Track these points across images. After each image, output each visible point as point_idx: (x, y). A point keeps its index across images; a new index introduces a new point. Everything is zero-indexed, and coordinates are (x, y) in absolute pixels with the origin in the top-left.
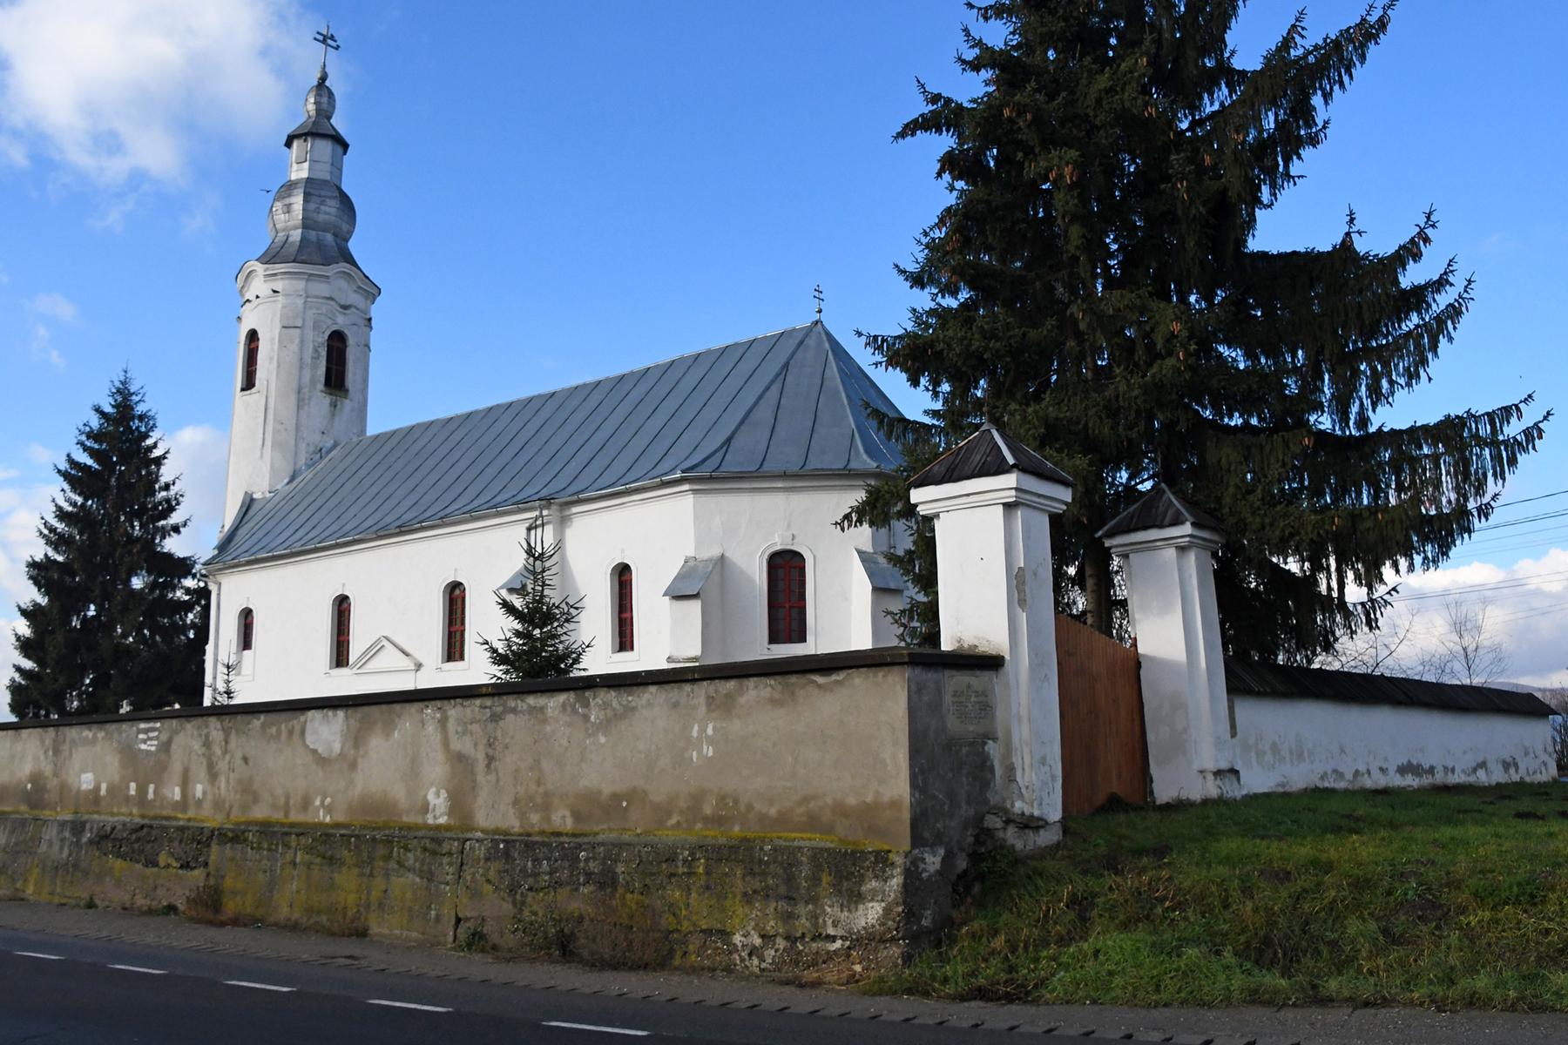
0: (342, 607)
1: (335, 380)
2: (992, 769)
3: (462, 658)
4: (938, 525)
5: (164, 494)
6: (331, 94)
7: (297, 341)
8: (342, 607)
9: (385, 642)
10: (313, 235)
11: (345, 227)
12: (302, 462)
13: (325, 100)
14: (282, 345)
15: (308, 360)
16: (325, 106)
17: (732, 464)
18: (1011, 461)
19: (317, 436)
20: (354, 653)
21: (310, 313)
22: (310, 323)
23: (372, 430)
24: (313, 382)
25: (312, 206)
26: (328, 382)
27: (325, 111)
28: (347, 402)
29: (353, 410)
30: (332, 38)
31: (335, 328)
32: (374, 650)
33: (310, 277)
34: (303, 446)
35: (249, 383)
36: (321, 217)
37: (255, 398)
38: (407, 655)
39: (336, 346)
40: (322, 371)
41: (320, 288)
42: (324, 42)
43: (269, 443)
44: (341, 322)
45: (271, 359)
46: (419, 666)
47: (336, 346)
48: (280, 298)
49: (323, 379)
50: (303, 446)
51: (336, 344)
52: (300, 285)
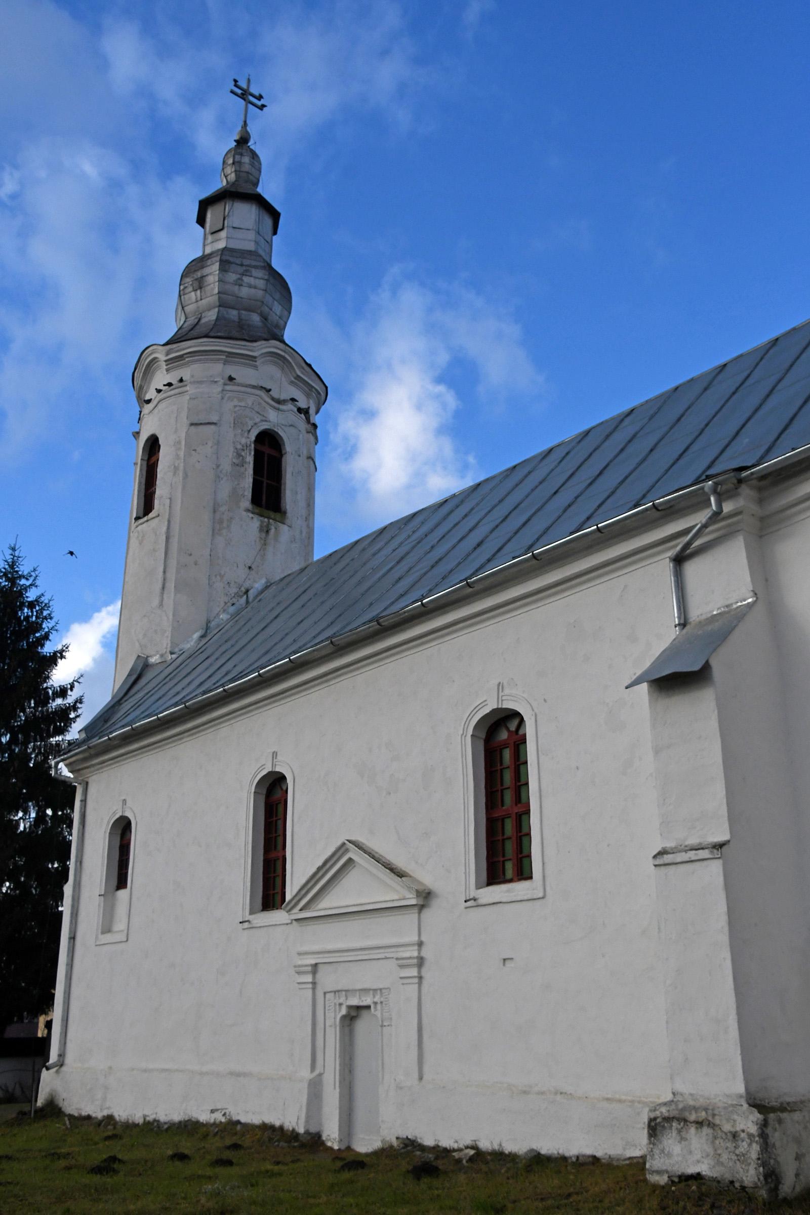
0: (273, 793)
1: (268, 496)
3: (523, 873)
5: (59, 701)
6: (254, 155)
8: (273, 793)
9: (353, 853)
10: (233, 314)
11: (278, 309)
13: (246, 160)
14: (191, 449)
15: (226, 466)
16: (247, 167)
18: (66, 1119)
19: (242, 573)
20: (297, 875)
23: (318, 555)
24: (235, 495)
25: (232, 277)
26: (256, 500)
28: (284, 528)
29: (293, 540)
31: (264, 426)
32: (335, 867)
35: (147, 505)
36: (245, 292)
37: (155, 525)
38: (399, 874)
39: (268, 453)
40: (248, 482)
43: (171, 585)
44: (274, 419)
45: (176, 469)
46: (426, 897)
47: (268, 453)
49: (249, 494)
51: (266, 450)
52: (217, 369)
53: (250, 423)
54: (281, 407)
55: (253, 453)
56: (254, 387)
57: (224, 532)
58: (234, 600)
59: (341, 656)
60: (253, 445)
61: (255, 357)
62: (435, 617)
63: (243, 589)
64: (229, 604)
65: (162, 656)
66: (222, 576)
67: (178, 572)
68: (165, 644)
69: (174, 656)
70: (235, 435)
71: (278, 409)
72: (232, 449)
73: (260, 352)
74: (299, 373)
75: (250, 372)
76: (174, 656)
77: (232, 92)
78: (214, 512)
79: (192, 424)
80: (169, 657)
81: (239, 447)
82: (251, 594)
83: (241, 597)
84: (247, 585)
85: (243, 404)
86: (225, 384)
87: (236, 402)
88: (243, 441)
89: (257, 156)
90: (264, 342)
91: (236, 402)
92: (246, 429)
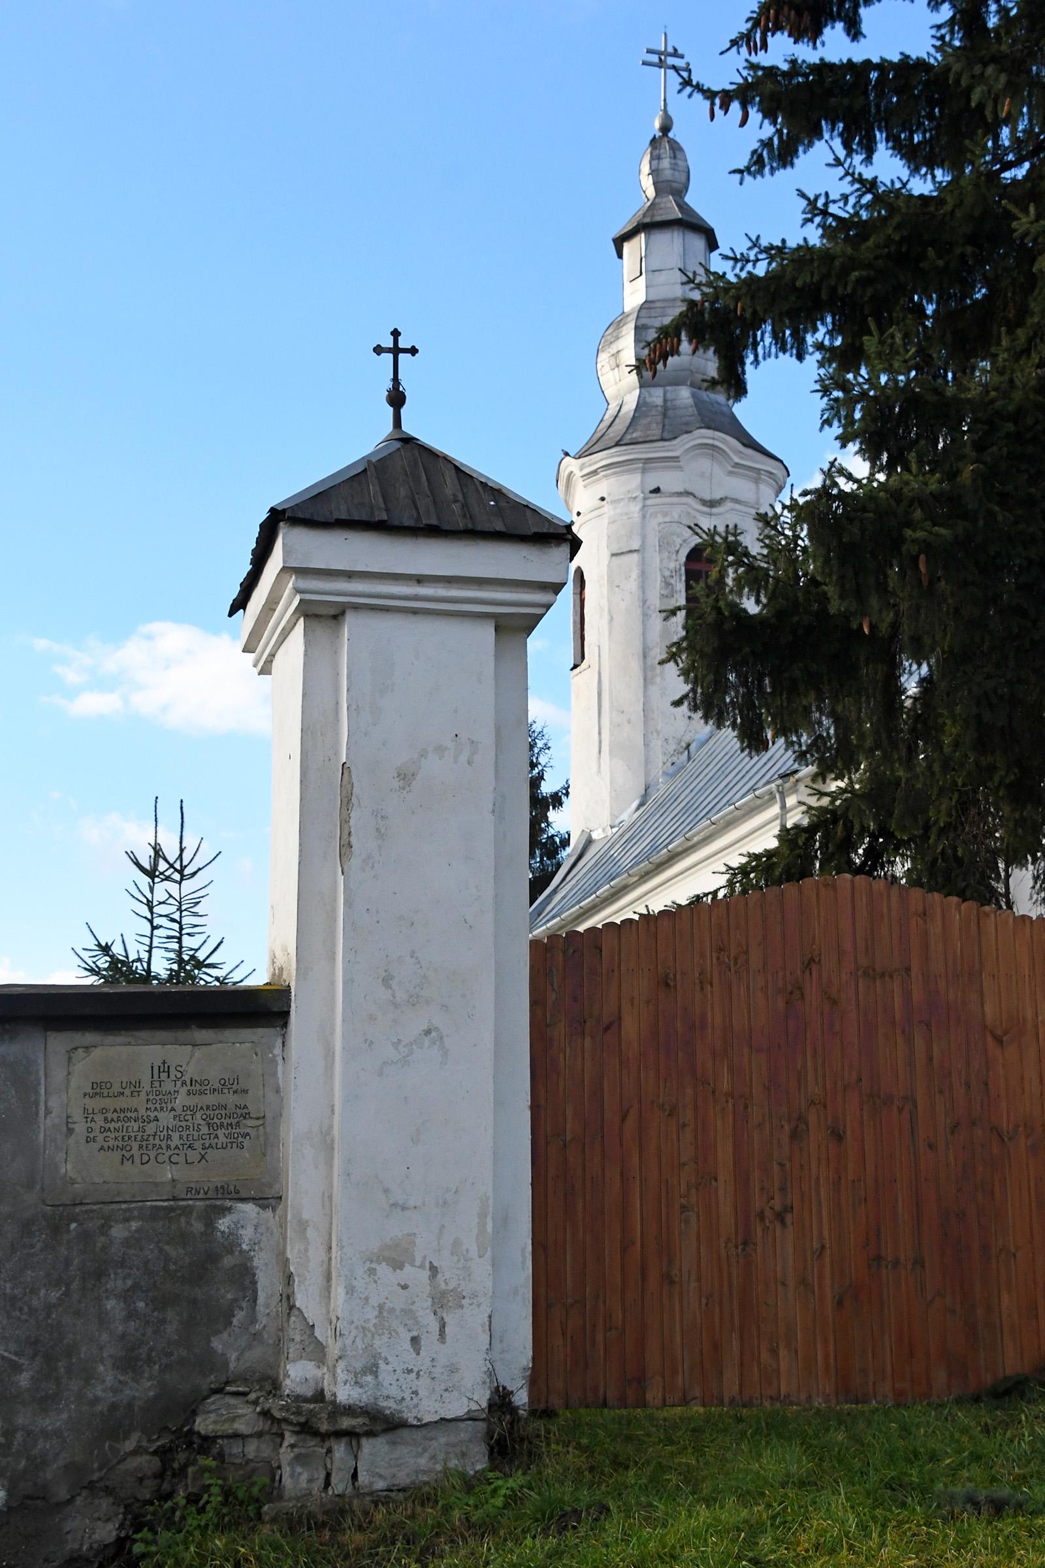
2: (159, 1447)
4: (575, 529)
7: (635, 574)
12: (657, 769)
16: (668, 174)
17: (321, 514)
21: (653, 523)
22: (653, 540)
27: (672, 186)
30: (676, 54)
33: (647, 464)
34: (657, 743)
37: (585, 679)
41: (669, 480)
42: (661, 64)
48: (607, 508)
50: (657, 743)
52: (632, 482)
53: (678, 541)
54: (714, 510)
55: (684, 578)
56: (679, 494)
57: (658, 680)
58: (674, 759)
59: (645, 882)
60: (683, 569)
61: (676, 459)
62: (683, 858)
63: (684, 745)
64: (669, 764)
65: (604, 830)
66: (658, 733)
67: (612, 734)
68: (605, 818)
69: (615, 830)
70: (661, 561)
71: (711, 515)
72: (659, 578)
73: (682, 450)
74: (737, 460)
75: (677, 474)
76: (615, 830)
77: (644, 63)
78: (645, 657)
79: (613, 555)
80: (610, 832)
81: (667, 573)
82: (693, 748)
83: (682, 753)
84: (687, 739)
85: (667, 519)
86: (645, 499)
87: (660, 519)
88: (672, 565)
89: (681, 149)
90: (685, 436)
91: (660, 519)
92: (673, 550)
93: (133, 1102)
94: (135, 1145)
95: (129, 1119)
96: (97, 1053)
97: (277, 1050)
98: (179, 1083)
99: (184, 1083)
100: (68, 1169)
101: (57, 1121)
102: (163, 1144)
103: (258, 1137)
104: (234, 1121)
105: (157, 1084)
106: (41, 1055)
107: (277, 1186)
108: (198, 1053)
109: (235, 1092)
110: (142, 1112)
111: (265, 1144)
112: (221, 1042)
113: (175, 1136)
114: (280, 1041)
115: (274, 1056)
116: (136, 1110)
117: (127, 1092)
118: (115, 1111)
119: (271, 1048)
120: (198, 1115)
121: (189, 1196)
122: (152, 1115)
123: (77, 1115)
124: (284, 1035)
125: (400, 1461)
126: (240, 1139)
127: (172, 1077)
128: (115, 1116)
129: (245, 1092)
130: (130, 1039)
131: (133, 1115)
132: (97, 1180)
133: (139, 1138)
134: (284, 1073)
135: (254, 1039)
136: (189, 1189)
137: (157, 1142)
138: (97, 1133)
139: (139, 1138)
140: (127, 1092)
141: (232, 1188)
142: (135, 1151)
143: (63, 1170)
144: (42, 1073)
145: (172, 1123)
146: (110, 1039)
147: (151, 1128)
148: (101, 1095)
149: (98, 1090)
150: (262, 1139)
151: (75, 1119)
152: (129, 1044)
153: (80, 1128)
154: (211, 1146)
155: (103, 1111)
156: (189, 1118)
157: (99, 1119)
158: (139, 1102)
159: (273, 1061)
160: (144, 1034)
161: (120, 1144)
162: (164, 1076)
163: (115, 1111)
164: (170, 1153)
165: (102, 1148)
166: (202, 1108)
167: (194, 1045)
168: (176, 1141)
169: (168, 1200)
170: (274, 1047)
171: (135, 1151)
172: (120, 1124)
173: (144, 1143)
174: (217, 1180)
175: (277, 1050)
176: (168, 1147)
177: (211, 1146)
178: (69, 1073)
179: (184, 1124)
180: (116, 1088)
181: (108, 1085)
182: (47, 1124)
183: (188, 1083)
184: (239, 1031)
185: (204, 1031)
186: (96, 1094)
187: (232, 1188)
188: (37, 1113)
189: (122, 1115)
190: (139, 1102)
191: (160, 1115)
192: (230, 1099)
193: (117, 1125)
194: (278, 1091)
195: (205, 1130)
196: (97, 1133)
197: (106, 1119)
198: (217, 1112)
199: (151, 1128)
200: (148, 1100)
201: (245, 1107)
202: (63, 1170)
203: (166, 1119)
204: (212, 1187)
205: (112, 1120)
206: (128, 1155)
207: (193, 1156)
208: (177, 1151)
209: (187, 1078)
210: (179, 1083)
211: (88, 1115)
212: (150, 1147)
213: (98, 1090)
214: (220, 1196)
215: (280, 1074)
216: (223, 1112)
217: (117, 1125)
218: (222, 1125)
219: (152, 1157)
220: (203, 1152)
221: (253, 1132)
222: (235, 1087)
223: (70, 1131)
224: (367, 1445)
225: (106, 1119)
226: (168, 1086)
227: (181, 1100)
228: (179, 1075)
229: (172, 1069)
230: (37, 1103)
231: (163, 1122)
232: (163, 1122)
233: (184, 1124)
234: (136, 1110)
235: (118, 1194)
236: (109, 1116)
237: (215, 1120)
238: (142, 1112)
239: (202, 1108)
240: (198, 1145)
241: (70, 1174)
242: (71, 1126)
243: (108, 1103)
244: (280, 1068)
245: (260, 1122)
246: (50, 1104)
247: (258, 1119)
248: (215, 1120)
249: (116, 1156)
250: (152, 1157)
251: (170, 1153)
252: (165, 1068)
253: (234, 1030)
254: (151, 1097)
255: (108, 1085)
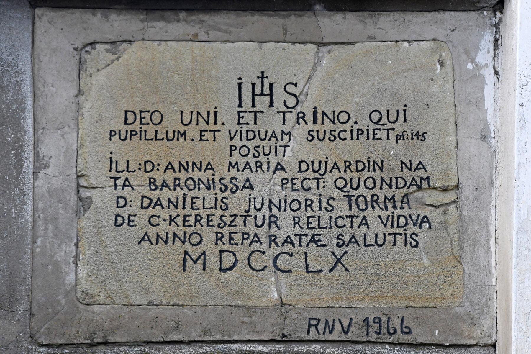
93: (205, 151)
94: (209, 234)
95: (198, 183)
96: (132, 54)
97: (484, 56)
98: (291, 117)
99: (301, 117)
100: (80, 276)
101: (56, 182)
102: (263, 233)
103: (445, 225)
104: (399, 194)
105: (249, 118)
106: (25, 55)
107: (485, 323)
108: (328, 59)
109: (400, 137)
110: (221, 170)
111: (460, 242)
112: (372, 39)
113: (285, 218)
114: (489, 37)
115: (478, 67)
116: (209, 167)
117: (193, 132)
118: (170, 166)
119: (470, 53)
120: (329, 179)
121: (313, 334)
122: (241, 177)
123: (98, 174)
124: (497, 26)
125: (54, 237)
126: (411, 229)
127: (278, 105)
128: (170, 177)
129: (421, 136)
130: (195, 29)
131: (205, 176)
132: (135, 299)
133: (216, 220)
134: (497, 100)
135: (440, 34)
136: (313, 323)
137: (251, 229)
138: (134, 208)
139: (216, 220)
140: (193, 132)
141: (396, 323)
142: (209, 245)
143: (71, 278)
144: (27, 89)
145: (278, 194)
146: (158, 27)
147: (238, 202)
148: (142, 135)
149: (137, 127)
150: (453, 228)
151: (93, 182)
152: (195, 38)
153: (103, 198)
154: (353, 240)
155: (149, 166)
156: (312, 184)
157: (139, 180)
158: (216, 152)
159: (476, 77)
160: (223, 19)
161: (180, 231)
162: (262, 102)
163: (170, 166)
164: (275, 250)
165: (145, 238)
166: (335, 166)
167: (321, 44)
168: (285, 228)
169: (273, 341)
170: (477, 49)
171: (209, 245)
172: (179, 193)
173: (226, 230)
174: (367, 307)
175: (484, 56)
176: (272, 239)
177: (353, 240)
178: (80, 92)
179: (301, 195)
180: (172, 124)
181: (156, 118)
182: (43, 186)
183: (309, 117)
184: (410, 16)
185: (338, 17)
186: (133, 133)
187: (396, 323)
188: (20, 164)
189: (183, 176)
190: (216, 152)
191: (255, 177)
192: (391, 151)
193: (172, 195)
194: (484, 137)
195: (342, 208)
196: (134, 208)
197: (152, 182)
198: (366, 174)
199: (238, 202)
200: (232, 149)
201: (421, 166)
202: (71, 278)
203: (267, 186)
204: (358, 319)
205: (164, 184)
206: (195, 252)
207: (321, 258)
208: (288, 248)
209: (307, 108)
210: (291, 117)
211: (119, 174)
212: (237, 238)
213: (136, 124)
214: (373, 337)
215: (489, 103)
216: (377, 175)
217: (172, 195)
218: (375, 200)
219: (242, 257)
220: (339, 252)
221: (435, 216)
222: (399, 127)
223: (84, 204)
224: (396, 200)
225: (152, 182)
226: (270, 122)
227: (297, 149)
228: (291, 101)
229: (278, 90)
230: (19, 148)
231: (261, 192)
232: (261, 192)
233: (301, 195)
234: (209, 167)
235: (177, 328)
236: (159, 176)
237: (362, 190)
238: (221, 170)
239: (335, 166)
240: (329, 237)
241: (84, 285)
242: (85, 193)
243: (156, 152)
244: (489, 92)
245: (451, 196)
246: (44, 150)
247: (445, 190)
248: (362, 190)
249: (174, 253)
250: (242, 257)
251: (275, 250)
252: (264, 88)
253: (397, 16)
254: (237, 142)
255: (156, 118)
